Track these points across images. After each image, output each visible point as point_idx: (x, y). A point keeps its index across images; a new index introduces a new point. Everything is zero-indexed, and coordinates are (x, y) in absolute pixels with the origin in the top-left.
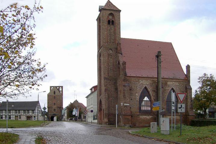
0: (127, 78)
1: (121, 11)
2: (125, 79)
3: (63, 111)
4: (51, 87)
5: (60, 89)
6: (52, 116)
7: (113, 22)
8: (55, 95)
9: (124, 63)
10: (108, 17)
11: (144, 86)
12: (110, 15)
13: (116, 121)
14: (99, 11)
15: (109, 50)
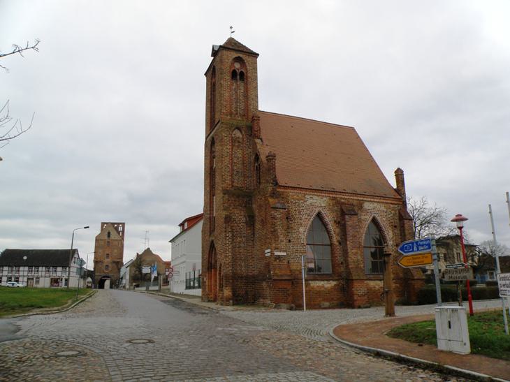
0: (278, 190)
1: (258, 55)
2: (274, 193)
3: (123, 270)
4: (103, 224)
5: (120, 229)
6: (101, 279)
7: (242, 74)
9: (271, 158)
10: (232, 64)
11: (317, 211)
12: (237, 62)
13: (303, 300)
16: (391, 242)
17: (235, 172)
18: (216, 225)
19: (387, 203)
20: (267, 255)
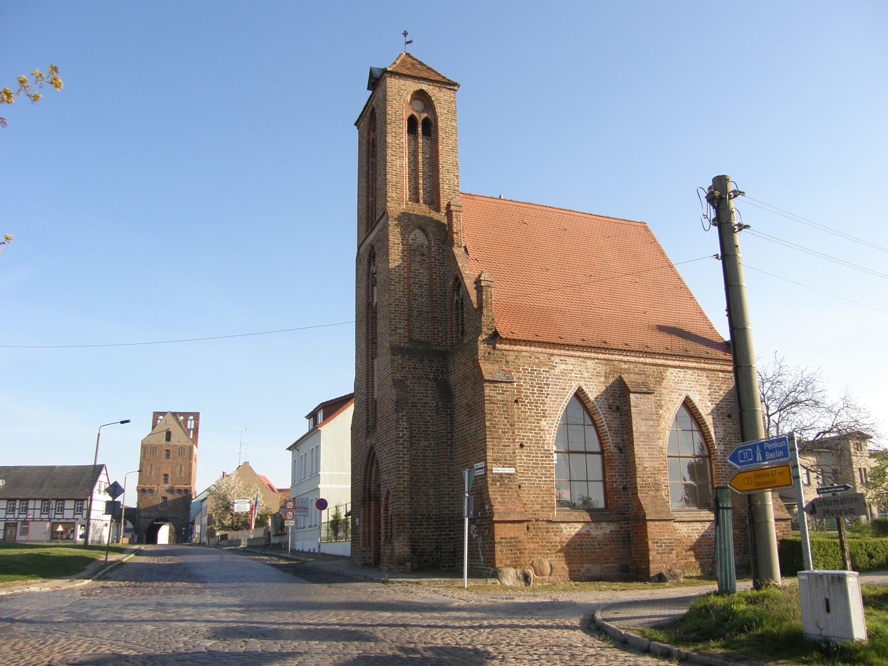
5: (191, 424)
8: (171, 443)
14: (368, 89)
18: (379, 415)
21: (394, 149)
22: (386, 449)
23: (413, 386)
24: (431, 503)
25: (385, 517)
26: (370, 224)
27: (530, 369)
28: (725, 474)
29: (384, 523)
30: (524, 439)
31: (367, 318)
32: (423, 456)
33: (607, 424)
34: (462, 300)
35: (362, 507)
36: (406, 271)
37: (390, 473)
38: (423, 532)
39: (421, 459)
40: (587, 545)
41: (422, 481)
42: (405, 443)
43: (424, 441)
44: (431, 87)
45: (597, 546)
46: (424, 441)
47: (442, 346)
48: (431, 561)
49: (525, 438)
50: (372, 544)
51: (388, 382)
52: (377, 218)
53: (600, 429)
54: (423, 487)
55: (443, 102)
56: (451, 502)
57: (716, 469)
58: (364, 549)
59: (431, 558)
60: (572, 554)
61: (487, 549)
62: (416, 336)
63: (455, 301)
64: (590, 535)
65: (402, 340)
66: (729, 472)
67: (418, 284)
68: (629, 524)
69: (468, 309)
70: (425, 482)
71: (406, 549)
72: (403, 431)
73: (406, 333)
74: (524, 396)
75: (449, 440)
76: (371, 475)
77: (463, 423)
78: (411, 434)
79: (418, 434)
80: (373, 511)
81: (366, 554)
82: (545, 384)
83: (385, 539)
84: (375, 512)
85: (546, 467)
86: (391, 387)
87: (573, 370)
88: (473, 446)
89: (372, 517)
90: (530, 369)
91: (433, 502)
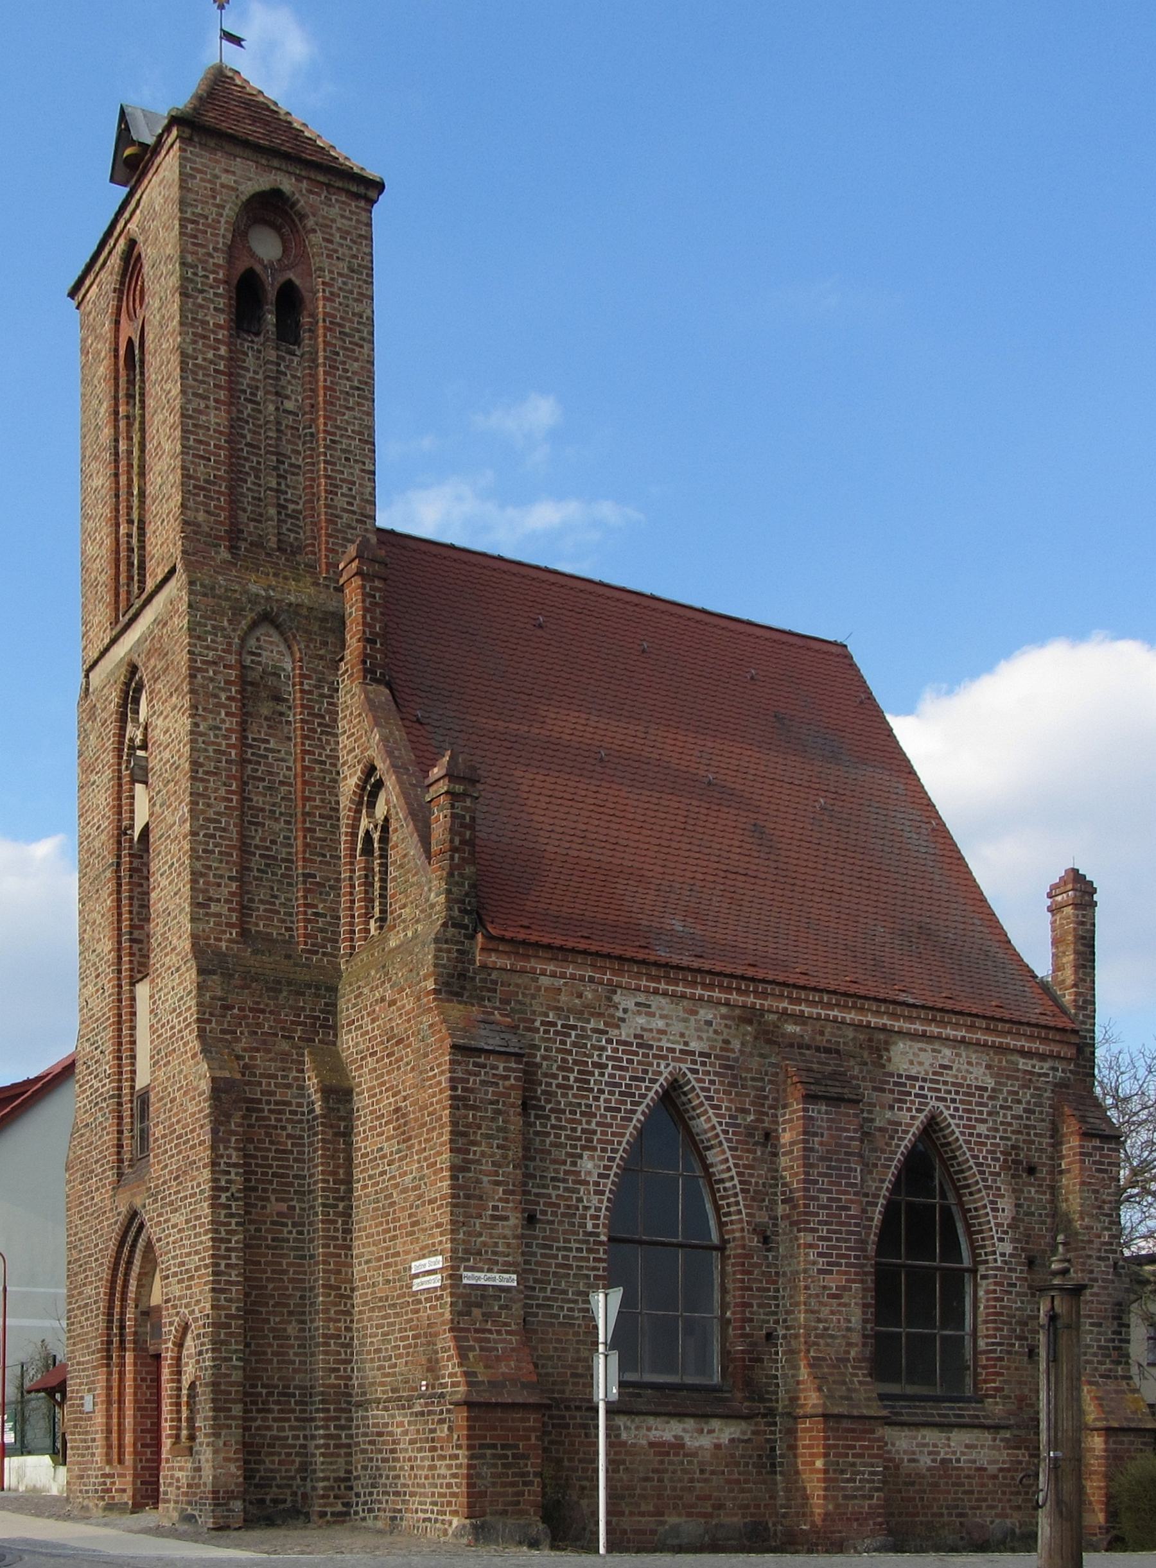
1: (380, 186)
10: (240, 234)
11: (665, 1072)
15: (254, 625)
16: (1007, 1248)
17: (256, 862)
18: (157, 1132)
19: (1002, 1050)
20: (418, 1285)
21: (200, 378)
22: (178, 1219)
23: (252, 1058)
24: (292, 1357)
25: (172, 1389)
26: (122, 605)
27: (559, 1023)
28: (1008, 1316)
29: (171, 1404)
30: (538, 1204)
31: (118, 871)
32: (273, 1240)
33: (738, 1174)
34: (385, 829)
35: (102, 1365)
36: (233, 741)
37: (191, 1278)
38: (269, 1428)
39: (267, 1247)
40: (674, 1472)
41: (271, 1303)
42: (233, 1204)
43: (277, 1200)
44: (304, 185)
45: (697, 1475)
46: (277, 1200)
47: (324, 954)
48: (289, 1499)
49: (542, 1201)
50: (128, 1458)
51: (185, 1045)
52: (150, 585)
53: (721, 1186)
54: (272, 1318)
55: (337, 239)
56: (343, 1356)
57: (988, 1300)
58: (107, 1470)
59: (288, 1492)
60: (638, 1491)
61: (443, 1471)
62: (257, 925)
63: (361, 834)
64: (682, 1446)
65: (224, 932)
66: (1017, 1309)
67: (264, 780)
68: (775, 1424)
69: (405, 856)
70: (276, 1305)
71: (233, 1468)
72: (229, 1173)
73: (234, 915)
74: (544, 1092)
75: (342, 1199)
76: (125, 1285)
77: (383, 1157)
78: (246, 1180)
79: (263, 1182)
80: (129, 1376)
81: (113, 1483)
82: (595, 1065)
83: (174, 1444)
84: (135, 1379)
85: (588, 1277)
86: (194, 1056)
87: (663, 1032)
88: (410, 1216)
89: (129, 1391)
90: (559, 1023)
91: (296, 1354)
